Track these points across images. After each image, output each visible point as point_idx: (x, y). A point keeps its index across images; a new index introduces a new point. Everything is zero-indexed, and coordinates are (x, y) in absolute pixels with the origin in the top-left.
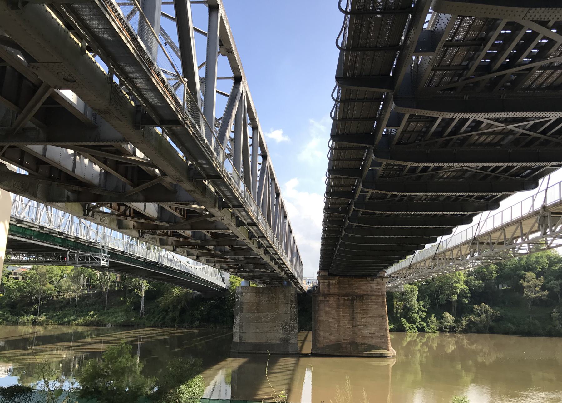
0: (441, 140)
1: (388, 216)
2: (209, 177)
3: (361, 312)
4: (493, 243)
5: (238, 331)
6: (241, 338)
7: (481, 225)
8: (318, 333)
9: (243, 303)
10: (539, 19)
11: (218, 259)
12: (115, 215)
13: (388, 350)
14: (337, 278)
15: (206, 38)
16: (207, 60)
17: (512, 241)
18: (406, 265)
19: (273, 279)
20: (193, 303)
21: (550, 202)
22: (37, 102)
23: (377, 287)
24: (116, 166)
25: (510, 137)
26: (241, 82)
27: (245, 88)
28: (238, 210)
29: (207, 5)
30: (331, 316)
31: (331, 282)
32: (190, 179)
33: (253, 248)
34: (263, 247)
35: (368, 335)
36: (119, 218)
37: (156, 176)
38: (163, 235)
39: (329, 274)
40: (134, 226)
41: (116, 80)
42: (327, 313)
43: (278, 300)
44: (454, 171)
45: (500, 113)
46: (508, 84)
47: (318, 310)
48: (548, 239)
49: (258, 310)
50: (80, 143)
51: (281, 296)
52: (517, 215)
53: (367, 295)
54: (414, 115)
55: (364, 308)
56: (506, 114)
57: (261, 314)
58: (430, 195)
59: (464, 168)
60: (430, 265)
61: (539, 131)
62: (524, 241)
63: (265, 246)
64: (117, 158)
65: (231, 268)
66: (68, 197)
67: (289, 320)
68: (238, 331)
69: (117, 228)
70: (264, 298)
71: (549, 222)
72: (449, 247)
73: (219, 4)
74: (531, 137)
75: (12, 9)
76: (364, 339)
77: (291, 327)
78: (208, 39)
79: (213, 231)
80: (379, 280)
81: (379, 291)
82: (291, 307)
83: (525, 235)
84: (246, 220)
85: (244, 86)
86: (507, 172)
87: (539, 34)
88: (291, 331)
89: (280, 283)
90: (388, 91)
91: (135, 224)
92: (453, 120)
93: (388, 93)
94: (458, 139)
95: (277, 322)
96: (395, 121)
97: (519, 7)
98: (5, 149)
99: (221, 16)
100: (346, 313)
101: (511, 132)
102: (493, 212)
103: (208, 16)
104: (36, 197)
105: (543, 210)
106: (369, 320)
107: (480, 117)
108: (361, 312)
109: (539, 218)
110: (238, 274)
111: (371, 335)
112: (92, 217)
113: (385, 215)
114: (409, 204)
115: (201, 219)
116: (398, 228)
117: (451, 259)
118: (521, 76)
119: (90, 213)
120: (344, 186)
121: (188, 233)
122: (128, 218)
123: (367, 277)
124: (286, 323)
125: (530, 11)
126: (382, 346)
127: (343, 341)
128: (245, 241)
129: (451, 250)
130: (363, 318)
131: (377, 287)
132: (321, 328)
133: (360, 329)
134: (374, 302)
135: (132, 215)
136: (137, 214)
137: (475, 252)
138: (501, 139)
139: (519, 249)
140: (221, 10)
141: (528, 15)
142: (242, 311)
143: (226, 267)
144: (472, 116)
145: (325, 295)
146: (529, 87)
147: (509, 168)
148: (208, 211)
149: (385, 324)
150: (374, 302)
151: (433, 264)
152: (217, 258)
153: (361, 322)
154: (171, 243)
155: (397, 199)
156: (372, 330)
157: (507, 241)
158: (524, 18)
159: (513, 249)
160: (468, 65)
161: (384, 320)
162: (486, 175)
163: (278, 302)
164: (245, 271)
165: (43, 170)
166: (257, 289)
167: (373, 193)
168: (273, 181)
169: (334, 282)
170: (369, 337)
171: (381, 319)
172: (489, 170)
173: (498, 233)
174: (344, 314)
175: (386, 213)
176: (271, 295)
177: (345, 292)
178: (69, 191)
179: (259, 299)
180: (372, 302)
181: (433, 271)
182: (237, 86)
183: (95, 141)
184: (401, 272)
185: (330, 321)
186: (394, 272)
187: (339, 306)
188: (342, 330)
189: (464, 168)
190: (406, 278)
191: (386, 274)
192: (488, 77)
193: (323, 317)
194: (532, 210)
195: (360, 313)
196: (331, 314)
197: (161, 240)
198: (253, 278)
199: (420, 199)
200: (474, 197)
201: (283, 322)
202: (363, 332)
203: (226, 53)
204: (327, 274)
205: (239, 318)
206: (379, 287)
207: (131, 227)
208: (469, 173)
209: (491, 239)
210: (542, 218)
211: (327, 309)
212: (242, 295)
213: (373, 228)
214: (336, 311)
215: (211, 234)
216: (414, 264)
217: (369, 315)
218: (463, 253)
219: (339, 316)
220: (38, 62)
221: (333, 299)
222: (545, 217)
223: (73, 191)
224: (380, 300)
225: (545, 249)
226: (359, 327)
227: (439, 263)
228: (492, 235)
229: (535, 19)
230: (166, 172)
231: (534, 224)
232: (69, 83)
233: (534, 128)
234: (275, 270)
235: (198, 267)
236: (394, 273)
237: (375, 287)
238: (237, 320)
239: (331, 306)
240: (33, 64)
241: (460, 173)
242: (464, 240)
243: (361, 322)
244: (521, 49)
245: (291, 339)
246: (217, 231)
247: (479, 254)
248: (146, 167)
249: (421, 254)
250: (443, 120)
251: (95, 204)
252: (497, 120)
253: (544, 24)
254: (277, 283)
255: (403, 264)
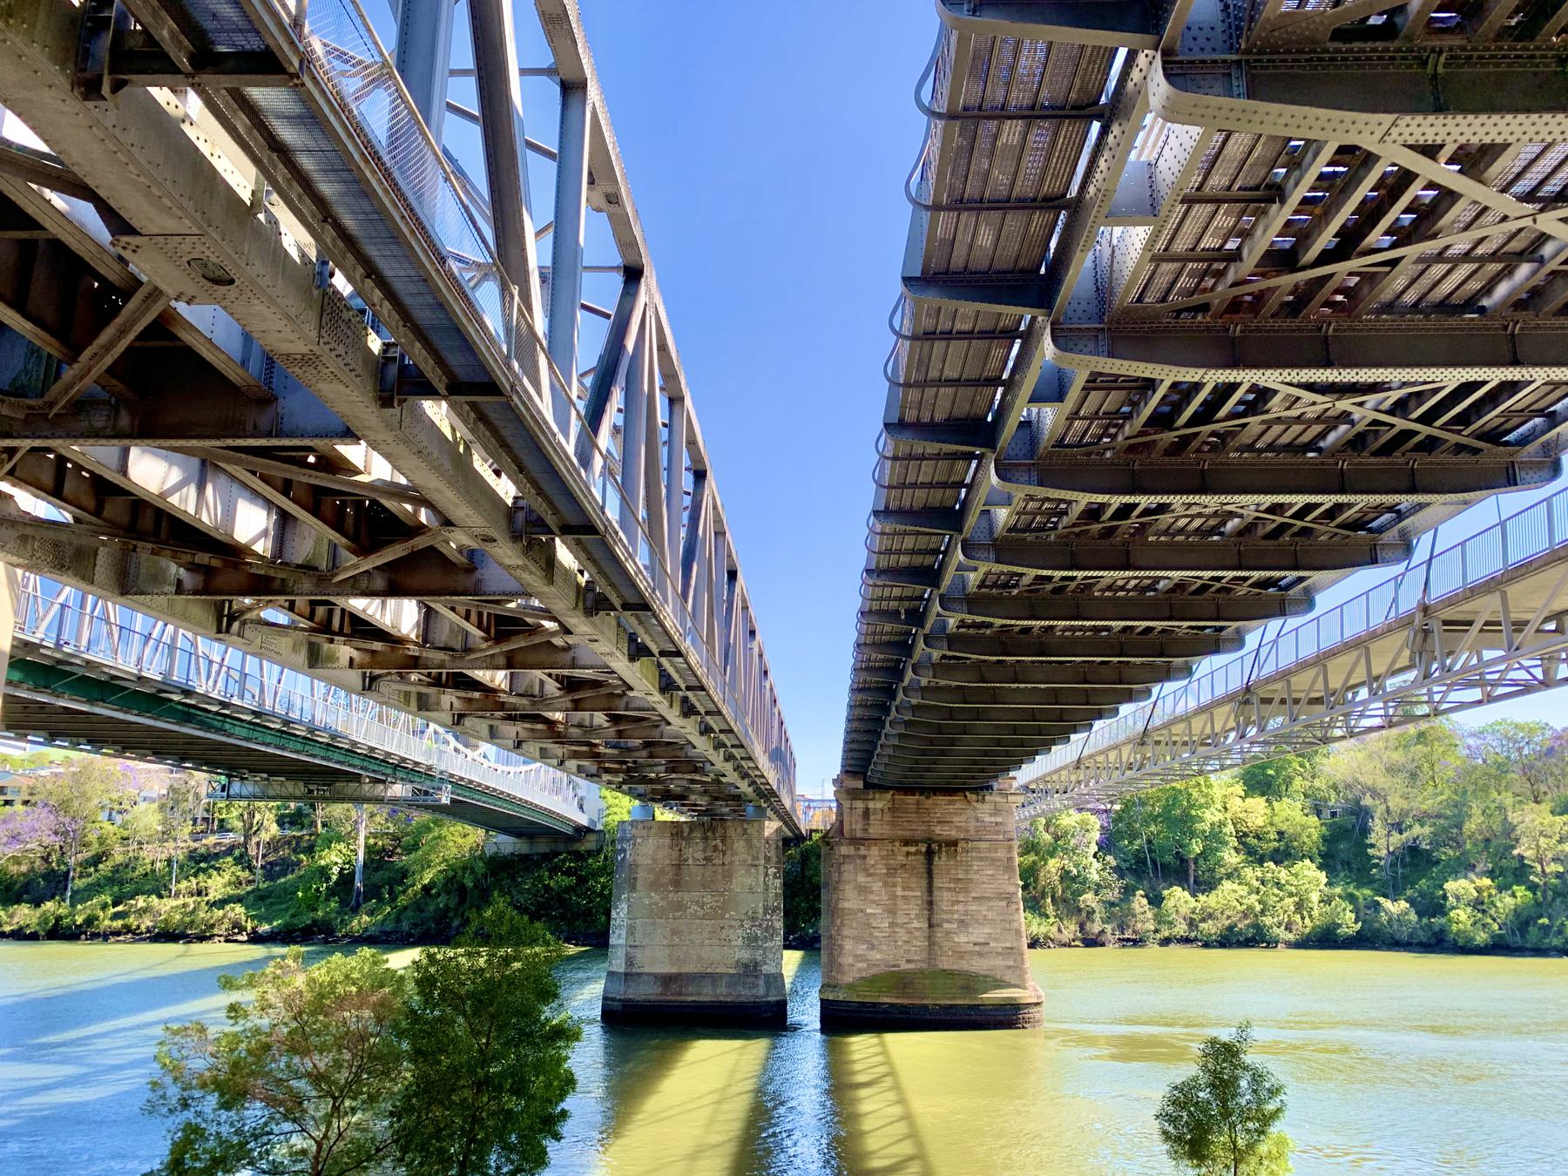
0: (1169, 437)
1: (1027, 630)
2: (566, 530)
3: (952, 885)
4: (1296, 701)
5: (622, 941)
6: (630, 961)
7: (1264, 652)
8: (840, 946)
9: (637, 866)
10: (1421, 142)
11: (574, 748)
12: (303, 629)
13: (1025, 988)
14: (889, 795)
15: (554, 165)
16: (556, 217)
17: (1344, 697)
18: (1069, 761)
19: (716, 799)
20: (499, 868)
21: (1438, 591)
22: (123, 332)
23: (993, 819)
24: (316, 501)
25: (1343, 428)
26: (643, 280)
27: (651, 297)
28: (637, 617)
29: (558, 79)
30: (872, 897)
31: (871, 805)
32: (515, 537)
33: (669, 718)
34: (698, 713)
35: (970, 947)
36: (313, 639)
37: (420, 529)
38: (429, 685)
39: (868, 786)
40: (351, 660)
41: (341, 283)
42: (863, 890)
43: (732, 855)
44: (1200, 515)
45: (1322, 371)
46: (1339, 298)
47: (838, 882)
48: (1436, 689)
49: (677, 884)
50: (230, 442)
51: (740, 845)
52: (1355, 627)
53: (966, 840)
54: (1101, 374)
55: (961, 876)
56: (1335, 372)
57: (686, 896)
58: (1136, 578)
59: (1226, 508)
60: (1132, 760)
61: (1415, 415)
62: (1373, 694)
63: (702, 711)
64: (322, 479)
65: (607, 771)
66: (179, 582)
67: (761, 911)
68: (622, 941)
69: (306, 666)
70: (695, 852)
71: (1437, 646)
72: (1180, 709)
73: (589, 76)
74: (1395, 431)
75: (86, 97)
76: (962, 958)
77: (766, 930)
78: (559, 167)
79: (566, 672)
80: (998, 799)
81: (997, 828)
82: (766, 875)
83: (1377, 678)
84: (656, 643)
85: (648, 290)
86: (1333, 519)
87: (1417, 176)
88: (765, 939)
89: (735, 811)
90: (1036, 311)
91: (355, 654)
92: (1197, 387)
93: (1034, 319)
94: (1213, 434)
95: (727, 916)
96: (1054, 389)
97: (1374, 111)
98: (18, 456)
99: (594, 108)
100: (911, 889)
101: (1345, 417)
102: (1293, 622)
103: (559, 107)
104: (92, 583)
105: (1422, 614)
106: (974, 908)
107: (1269, 378)
108: (952, 885)
109: (1412, 634)
110: (625, 787)
111: (977, 948)
112: (239, 635)
113: (1017, 629)
114: (1077, 603)
115: (537, 640)
116: (1042, 662)
117: (1185, 744)
118: (1369, 279)
119: (236, 625)
120: (912, 552)
121: (498, 678)
122: (336, 638)
123: (967, 793)
124: (754, 919)
125: (1399, 122)
126: (1007, 978)
127: (904, 966)
128: (649, 698)
129: (1186, 718)
130: (958, 902)
131: (993, 819)
132: (846, 932)
133: (948, 933)
134: (986, 859)
135: (347, 630)
136: (361, 629)
137: (1248, 723)
138: (1320, 433)
139: (1362, 716)
140: (593, 93)
141: (1394, 131)
142: (633, 888)
143: (593, 768)
144: (1247, 377)
145: (856, 841)
146: (1389, 307)
147: (1337, 509)
148: (554, 619)
149: (1016, 917)
150: (986, 859)
151: (1138, 756)
152: (572, 743)
153: (951, 912)
154: (448, 706)
155: (1049, 587)
156: (978, 933)
157: (1333, 695)
158: (1382, 140)
159: (1346, 715)
160: (1239, 248)
161: (1014, 907)
162: (1283, 524)
163: (731, 863)
164: (644, 780)
165: (114, 509)
166: (675, 829)
167: (987, 574)
168: (720, 538)
169: (879, 805)
170: (971, 953)
171: (1004, 903)
172: (1289, 513)
173: (1309, 674)
174: (906, 893)
175: (1021, 623)
176: (714, 843)
177: (908, 833)
178: (180, 565)
179: (681, 855)
180: (981, 859)
181: (1139, 775)
182: (631, 291)
183: (269, 435)
184: (1055, 777)
185: (869, 911)
186: (1037, 779)
187: (892, 871)
188: (902, 934)
189: (1226, 508)
190: (1067, 795)
191: (1015, 784)
192: (1288, 280)
193: (850, 900)
194: (1392, 614)
195: (949, 889)
196: (872, 892)
197: (420, 695)
198: (666, 798)
199: (1109, 588)
200: (1249, 582)
201: (743, 917)
202: (956, 940)
203: (603, 203)
204: (860, 784)
205: (624, 906)
206: (999, 819)
207: (345, 661)
208: (1237, 520)
209: (1289, 691)
210: (1420, 637)
211: (861, 879)
212: (634, 845)
213: (985, 661)
214: (886, 884)
215: (557, 680)
216: (1091, 756)
217: (973, 895)
218: (1218, 728)
219: (894, 897)
220: (140, 234)
221: (876, 853)
222: (1426, 633)
223: (193, 568)
224: (1001, 854)
225: (1428, 715)
226: (945, 925)
227: (1154, 755)
228: (1294, 680)
229: (1411, 141)
230: (453, 518)
231: (1400, 651)
232: (216, 287)
233: (1400, 407)
234: (724, 775)
235: (512, 769)
236: (1036, 781)
237: (988, 819)
238: (620, 914)
239: (872, 871)
240: (125, 239)
241: (1212, 522)
242: (1220, 691)
243: (951, 912)
244: (1370, 214)
245: (765, 963)
246: (577, 673)
247: (1262, 730)
248: (395, 504)
249: (1107, 730)
250: (1175, 385)
251: (247, 601)
252: (1310, 387)
253: (1430, 151)
254: (727, 809)
255: (1060, 755)
